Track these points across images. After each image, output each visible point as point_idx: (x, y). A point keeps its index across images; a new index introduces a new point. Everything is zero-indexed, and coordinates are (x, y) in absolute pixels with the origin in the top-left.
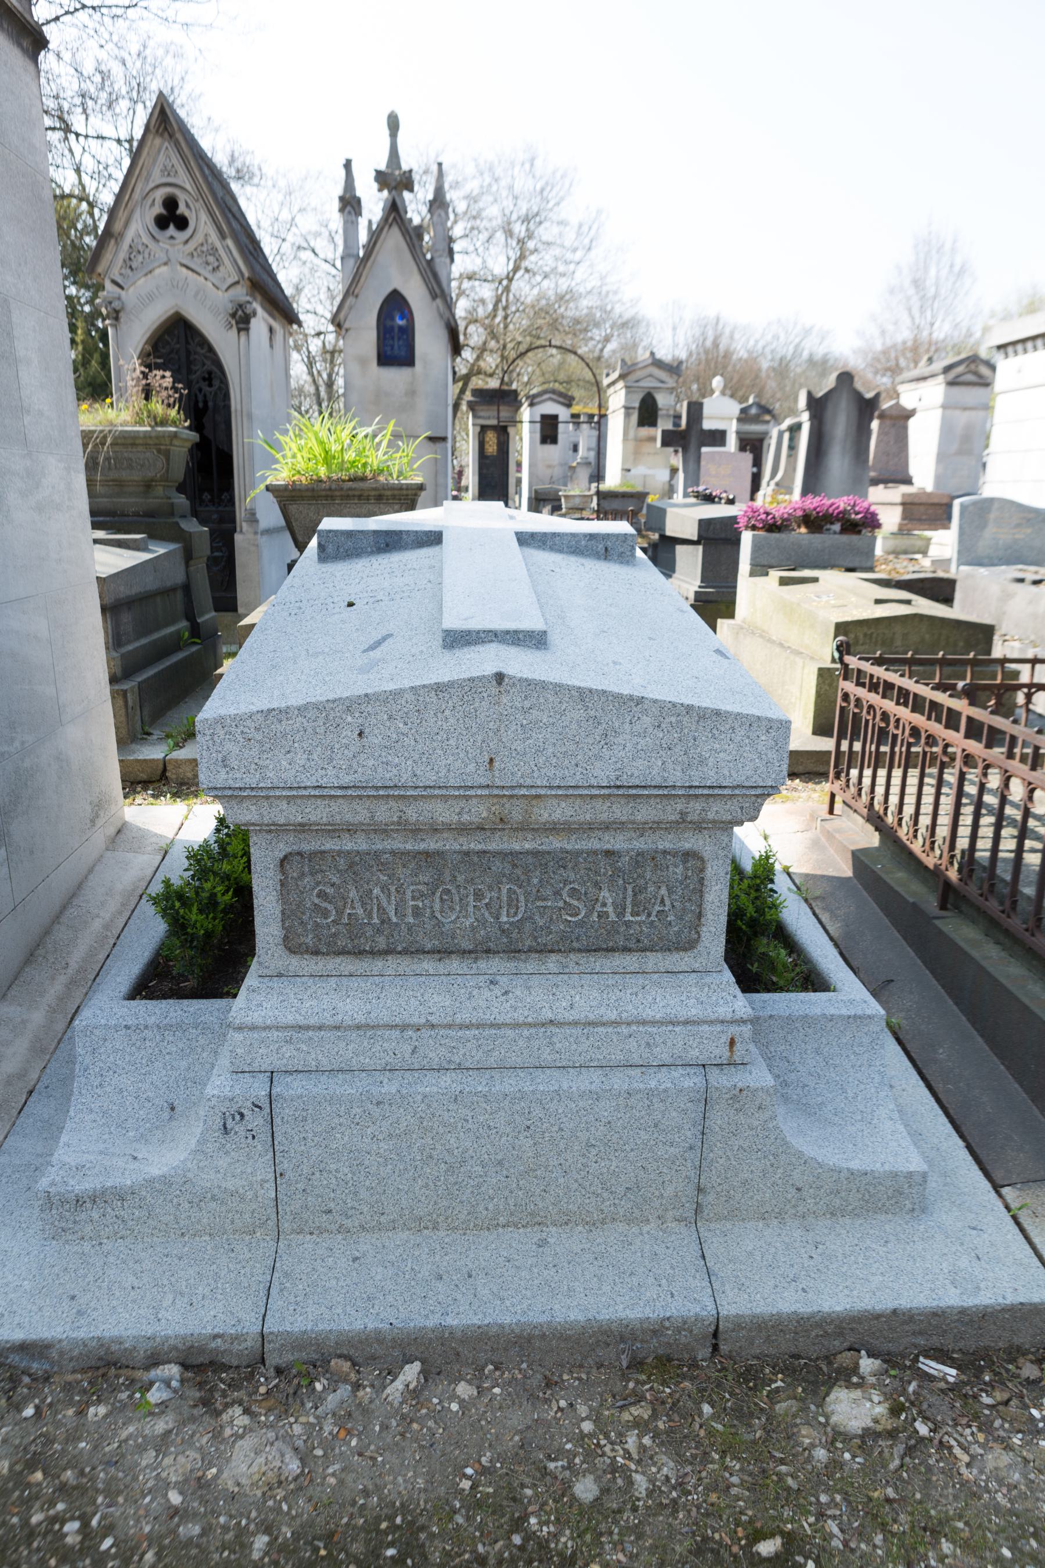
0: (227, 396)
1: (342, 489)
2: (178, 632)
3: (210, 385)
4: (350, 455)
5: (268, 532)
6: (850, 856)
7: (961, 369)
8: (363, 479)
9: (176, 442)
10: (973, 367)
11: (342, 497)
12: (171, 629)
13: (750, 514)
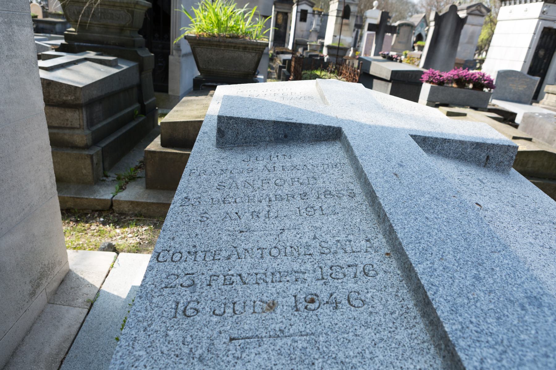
1: (225, 42)
2: (133, 111)
4: (231, 23)
5: (186, 55)
7: (474, 8)
8: (237, 37)
9: (137, 7)
10: (479, 8)
11: (225, 46)
12: (129, 109)
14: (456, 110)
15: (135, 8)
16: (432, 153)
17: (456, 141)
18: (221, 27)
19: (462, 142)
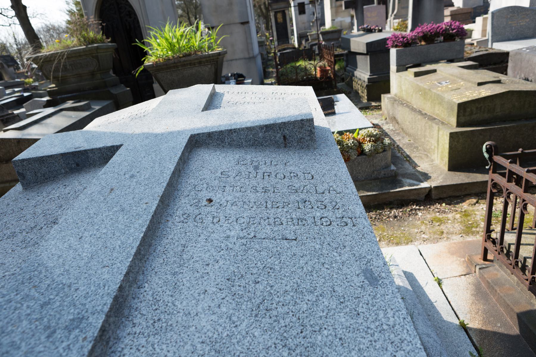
0: (138, 22)
1: (180, 62)
3: (130, 18)
4: (183, 43)
6: (516, 317)
13: (394, 39)
14: (428, 67)
15: (97, 53)
16: (223, 147)
17: (243, 129)
18: (174, 50)
19: (249, 129)
